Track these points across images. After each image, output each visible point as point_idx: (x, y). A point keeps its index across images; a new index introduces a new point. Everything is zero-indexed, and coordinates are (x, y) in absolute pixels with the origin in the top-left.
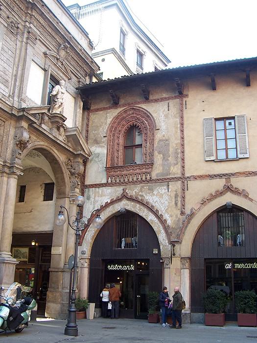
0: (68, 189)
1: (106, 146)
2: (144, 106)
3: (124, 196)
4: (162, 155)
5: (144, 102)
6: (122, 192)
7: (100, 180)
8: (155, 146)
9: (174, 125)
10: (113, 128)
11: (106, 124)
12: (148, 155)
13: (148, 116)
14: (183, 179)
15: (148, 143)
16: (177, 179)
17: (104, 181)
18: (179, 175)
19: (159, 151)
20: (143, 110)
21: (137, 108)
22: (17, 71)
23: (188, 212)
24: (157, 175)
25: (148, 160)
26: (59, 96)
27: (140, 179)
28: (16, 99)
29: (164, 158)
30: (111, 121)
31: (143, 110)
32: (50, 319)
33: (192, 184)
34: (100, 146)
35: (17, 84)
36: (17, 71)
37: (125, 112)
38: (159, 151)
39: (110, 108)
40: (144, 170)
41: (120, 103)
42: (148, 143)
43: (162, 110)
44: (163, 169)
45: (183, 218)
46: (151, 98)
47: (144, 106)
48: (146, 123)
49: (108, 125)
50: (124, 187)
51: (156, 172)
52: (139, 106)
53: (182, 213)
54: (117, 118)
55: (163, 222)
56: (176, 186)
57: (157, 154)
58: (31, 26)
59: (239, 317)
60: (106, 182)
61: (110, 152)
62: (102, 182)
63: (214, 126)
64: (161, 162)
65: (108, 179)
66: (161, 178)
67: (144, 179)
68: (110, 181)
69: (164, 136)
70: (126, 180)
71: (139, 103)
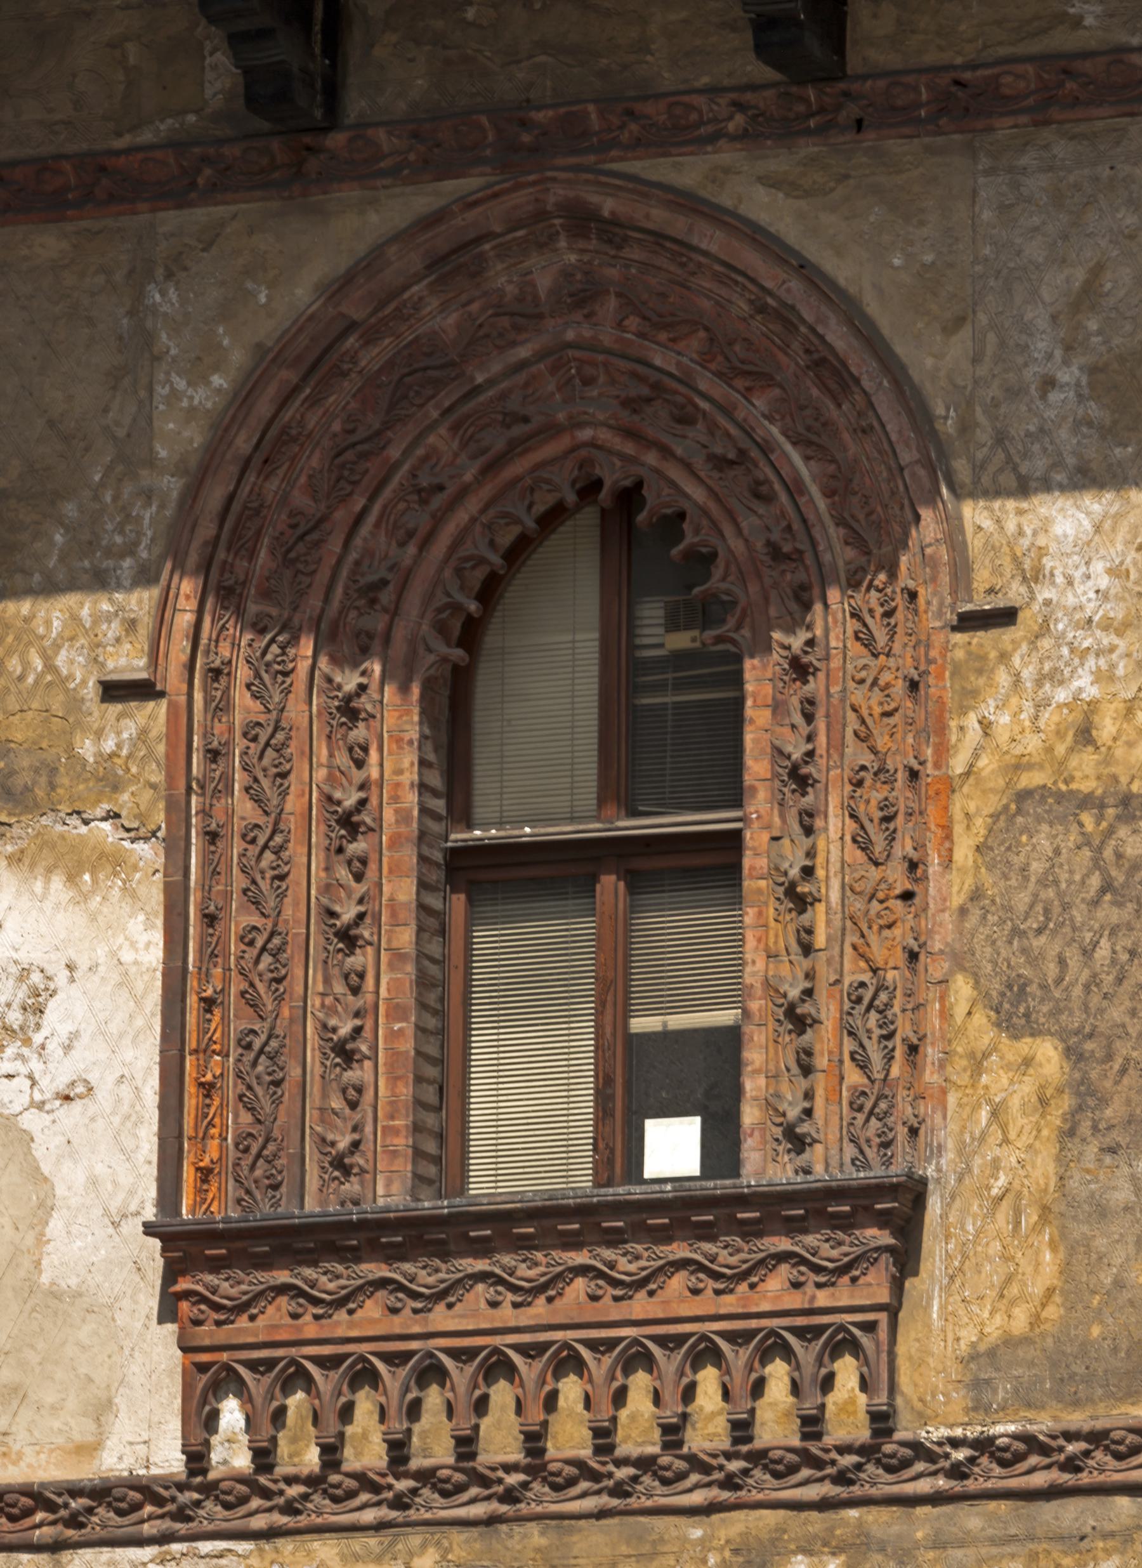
1: (148, 853)
2: (761, 189)
4: (1048, 1053)
5: (767, 129)
7: (82, 1430)
8: (951, 884)
9: (50, 1248)
11: (132, 456)
12: (826, 1039)
15: (835, 824)
17: (145, 1440)
19: (1017, 989)
20: (751, 259)
21: (658, 216)
24: (983, 1366)
25: (828, 1121)
29: (1086, 1095)
30: (222, 430)
31: (751, 259)
32: (944, 491)
34: (45, 842)
37: (454, 262)
38: (1017, 989)
39: (187, 175)
40: (774, 1290)
41: (355, 105)
42: (835, 824)
43: (1056, 285)
44: (1071, 1286)
48: (795, 489)
49: (172, 486)
52: (686, 171)
54: (310, 359)
55: (670, 375)
57: (981, 1029)
60: (168, 1459)
61: (211, 954)
62: (115, 1461)
64: (1044, 1168)
65: (200, 1421)
66: (1042, 1424)
68: (231, 1455)
69: (1085, 735)
70: (500, 1441)
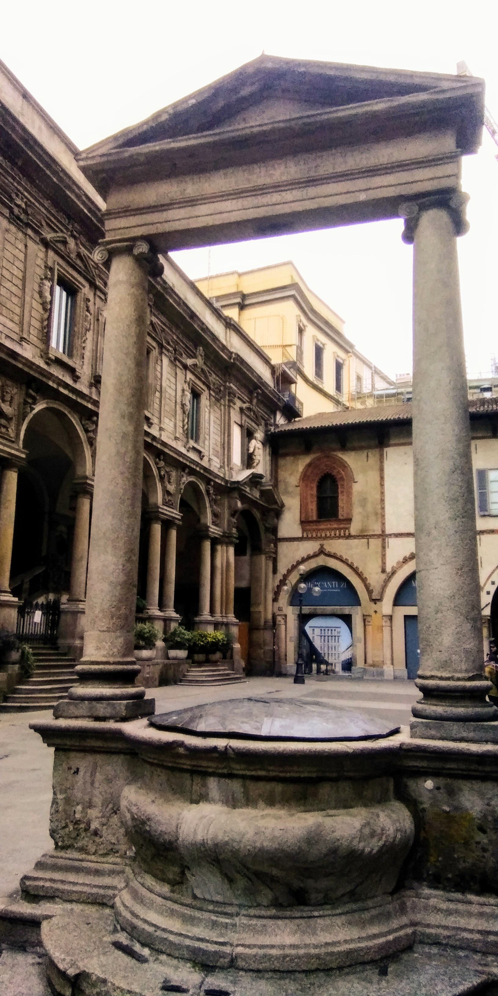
0: (263, 546)
3: (322, 552)
6: (319, 547)
10: (305, 477)
13: (344, 466)
14: (383, 536)
16: (379, 536)
18: (380, 532)
22: (224, 439)
23: (389, 569)
26: (256, 453)
27: (337, 535)
28: (226, 468)
33: (392, 542)
35: (226, 452)
36: (224, 439)
37: (318, 459)
39: (300, 454)
45: (384, 576)
46: (348, 445)
47: (340, 455)
50: (321, 542)
51: (354, 528)
53: (383, 571)
54: (309, 465)
56: (375, 543)
58: (231, 385)
59: (150, 698)
63: (335, 192)
65: (303, 533)
67: (342, 534)
71: (334, 450)
